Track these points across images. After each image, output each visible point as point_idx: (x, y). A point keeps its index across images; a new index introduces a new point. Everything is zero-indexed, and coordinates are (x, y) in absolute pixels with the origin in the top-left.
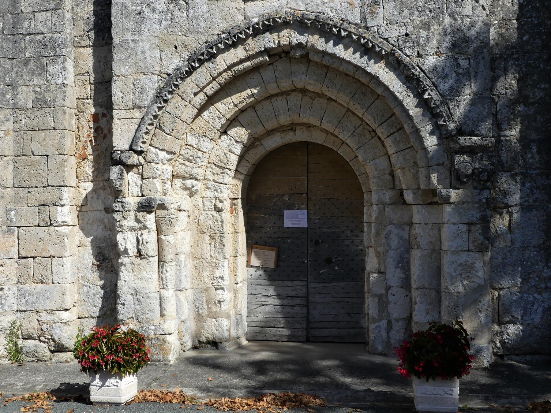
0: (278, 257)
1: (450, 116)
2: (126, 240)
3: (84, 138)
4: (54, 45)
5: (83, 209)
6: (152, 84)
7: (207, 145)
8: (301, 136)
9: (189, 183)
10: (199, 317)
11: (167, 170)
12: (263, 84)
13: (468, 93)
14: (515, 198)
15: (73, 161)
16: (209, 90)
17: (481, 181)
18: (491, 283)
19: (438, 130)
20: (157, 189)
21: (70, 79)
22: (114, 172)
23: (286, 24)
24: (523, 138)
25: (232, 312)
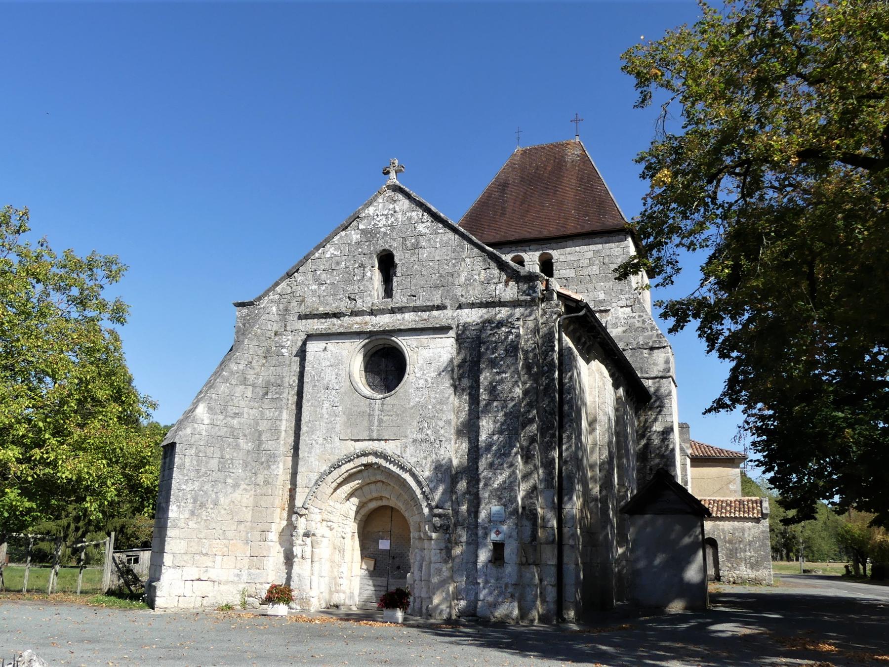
0: (375, 564)
1: (433, 499)
2: (297, 550)
3: (285, 500)
4: (273, 456)
5: (281, 534)
6: (314, 477)
7: (338, 505)
8: (384, 503)
9: (329, 524)
10: (331, 593)
11: (318, 518)
12: (363, 479)
13: (441, 489)
14: (464, 539)
15: (279, 510)
16: (339, 481)
17: (444, 529)
18: (451, 579)
19: (429, 505)
20: (313, 527)
21: (281, 470)
22: (294, 516)
23: (370, 454)
24: (468, 510)
25: (348, 591)
